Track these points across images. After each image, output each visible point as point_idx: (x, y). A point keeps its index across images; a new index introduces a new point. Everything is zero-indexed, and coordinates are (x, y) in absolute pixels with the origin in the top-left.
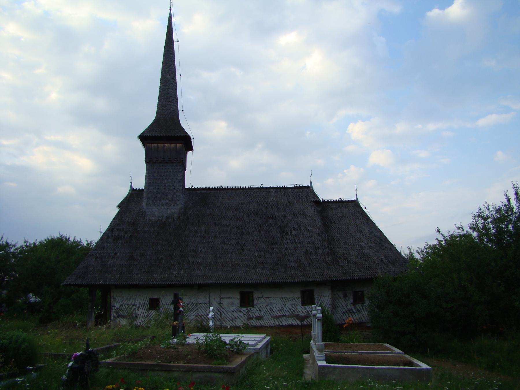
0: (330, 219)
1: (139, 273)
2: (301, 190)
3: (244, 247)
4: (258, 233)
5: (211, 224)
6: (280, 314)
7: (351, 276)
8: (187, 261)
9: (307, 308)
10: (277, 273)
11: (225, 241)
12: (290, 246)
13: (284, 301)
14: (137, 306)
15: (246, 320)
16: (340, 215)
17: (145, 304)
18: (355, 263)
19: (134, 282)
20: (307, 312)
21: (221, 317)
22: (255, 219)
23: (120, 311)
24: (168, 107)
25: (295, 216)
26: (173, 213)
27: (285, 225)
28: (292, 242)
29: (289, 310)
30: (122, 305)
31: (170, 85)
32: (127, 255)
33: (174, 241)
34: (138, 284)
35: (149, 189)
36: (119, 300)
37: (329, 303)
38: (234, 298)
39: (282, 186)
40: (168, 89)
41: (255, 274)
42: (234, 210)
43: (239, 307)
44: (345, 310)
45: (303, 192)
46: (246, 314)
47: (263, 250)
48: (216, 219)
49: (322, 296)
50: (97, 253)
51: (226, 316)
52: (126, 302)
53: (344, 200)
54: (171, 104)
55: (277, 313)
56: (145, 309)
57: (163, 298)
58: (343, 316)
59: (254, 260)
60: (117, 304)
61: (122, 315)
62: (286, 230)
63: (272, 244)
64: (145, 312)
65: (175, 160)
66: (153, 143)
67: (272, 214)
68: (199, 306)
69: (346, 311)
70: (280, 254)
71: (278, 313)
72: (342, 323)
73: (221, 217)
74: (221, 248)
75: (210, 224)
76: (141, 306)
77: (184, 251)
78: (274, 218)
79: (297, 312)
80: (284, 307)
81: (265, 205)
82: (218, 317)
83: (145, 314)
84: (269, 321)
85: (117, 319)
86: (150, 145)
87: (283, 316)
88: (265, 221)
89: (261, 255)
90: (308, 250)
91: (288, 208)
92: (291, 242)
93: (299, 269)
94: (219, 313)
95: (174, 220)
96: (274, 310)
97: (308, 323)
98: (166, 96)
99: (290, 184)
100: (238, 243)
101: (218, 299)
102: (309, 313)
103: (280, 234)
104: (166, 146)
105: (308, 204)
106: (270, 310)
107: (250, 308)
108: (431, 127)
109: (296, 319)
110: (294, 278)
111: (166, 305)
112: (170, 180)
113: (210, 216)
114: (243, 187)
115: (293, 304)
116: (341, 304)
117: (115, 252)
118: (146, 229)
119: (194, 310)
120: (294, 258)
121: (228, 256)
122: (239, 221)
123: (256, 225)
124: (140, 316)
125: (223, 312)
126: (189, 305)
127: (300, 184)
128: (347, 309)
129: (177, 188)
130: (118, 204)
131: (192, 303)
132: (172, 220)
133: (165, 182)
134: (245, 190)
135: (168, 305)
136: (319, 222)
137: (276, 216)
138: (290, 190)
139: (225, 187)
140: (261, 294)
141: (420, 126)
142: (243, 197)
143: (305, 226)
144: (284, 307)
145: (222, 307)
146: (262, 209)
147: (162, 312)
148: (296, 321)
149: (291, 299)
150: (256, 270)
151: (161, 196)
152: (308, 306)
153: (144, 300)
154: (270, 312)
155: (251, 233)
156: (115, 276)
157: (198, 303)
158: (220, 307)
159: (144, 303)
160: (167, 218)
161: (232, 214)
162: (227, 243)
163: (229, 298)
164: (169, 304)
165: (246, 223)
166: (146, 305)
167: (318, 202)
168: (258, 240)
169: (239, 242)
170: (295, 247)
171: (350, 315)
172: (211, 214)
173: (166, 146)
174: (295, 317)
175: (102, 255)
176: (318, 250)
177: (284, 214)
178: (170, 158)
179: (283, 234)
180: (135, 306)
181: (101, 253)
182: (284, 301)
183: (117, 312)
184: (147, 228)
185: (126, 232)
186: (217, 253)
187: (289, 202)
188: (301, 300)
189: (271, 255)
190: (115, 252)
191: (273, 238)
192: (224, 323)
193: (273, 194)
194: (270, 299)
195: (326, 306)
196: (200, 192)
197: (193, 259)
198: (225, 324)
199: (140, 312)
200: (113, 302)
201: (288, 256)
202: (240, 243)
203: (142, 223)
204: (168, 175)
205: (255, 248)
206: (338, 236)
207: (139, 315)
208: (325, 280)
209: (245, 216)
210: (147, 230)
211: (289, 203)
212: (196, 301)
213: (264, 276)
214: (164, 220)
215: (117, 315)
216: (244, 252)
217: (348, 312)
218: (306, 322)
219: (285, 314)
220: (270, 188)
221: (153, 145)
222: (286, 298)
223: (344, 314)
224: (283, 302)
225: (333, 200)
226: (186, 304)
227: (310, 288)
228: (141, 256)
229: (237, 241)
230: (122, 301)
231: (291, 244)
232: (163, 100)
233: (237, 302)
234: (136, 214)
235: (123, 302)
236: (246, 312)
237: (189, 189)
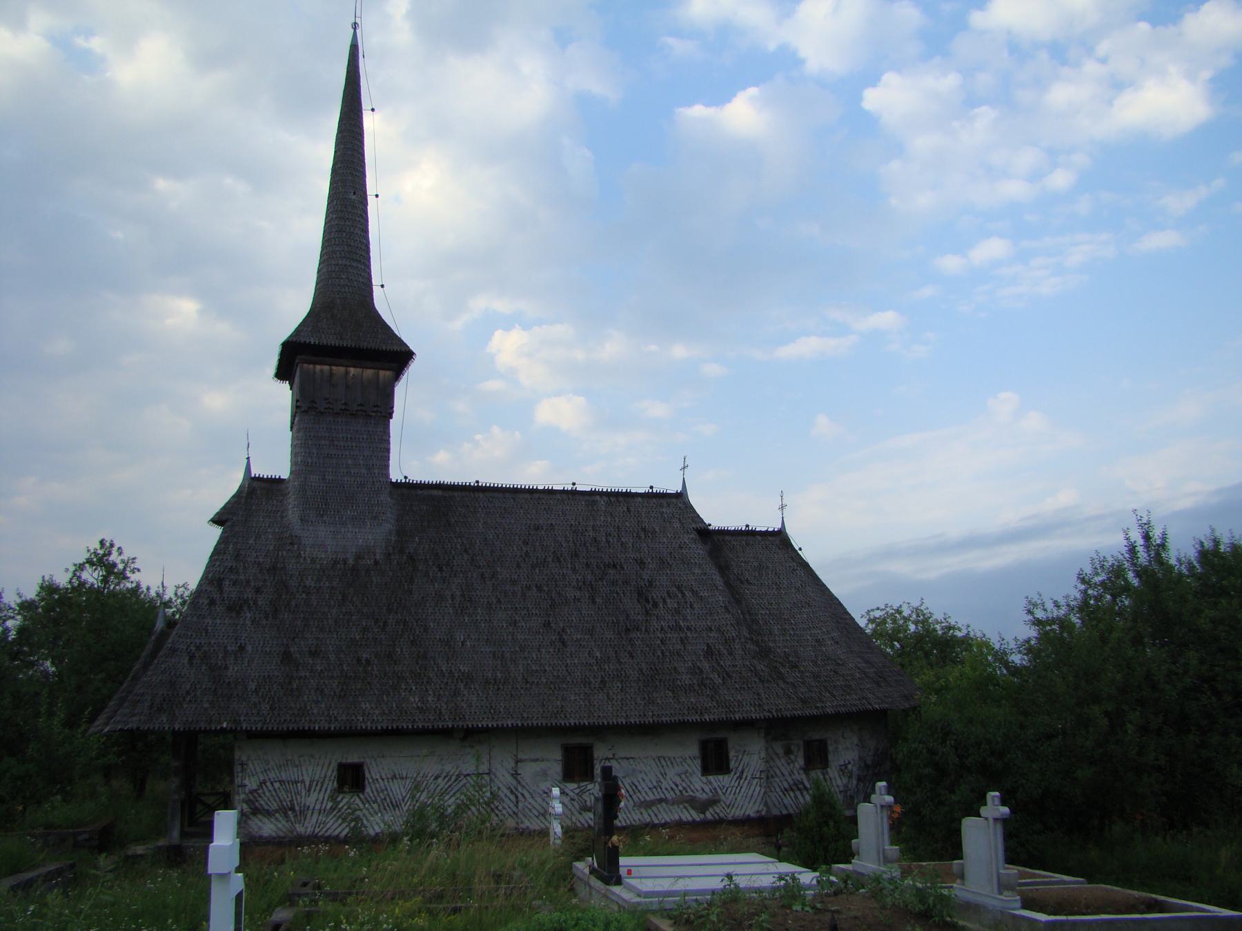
0: (735, 571)
1: (320, 699)
2: (664, 502)
5: (472, 577)
6: (654, 795)
7: (818, 707)
8: (436, 669)
9: (713, 780)
11: (516, 620)
12: (669, 635)
13: (663, 767)
14: (305, 785)
15: (576, 813)
16: (754, 563)
17: (325, 777)
18: (816, 677)
19: (314, 723)
20: (713, 791)
21: (517, 807)
22: (575, 568)
23: (259, 799)
24: (353, 273)
25: (664, 563)
26: (372, 544)
27: (647, 585)
28: (673, 625)
29: (674, 786)
30: (264, 782)
31: (357, 219)
32: (275, 651)
33: (391, 617)
34: (326, 728)
35: (308, 480)
36: (255, 769)
37: (760, 769)
38: (548, 760)
39: (620, 491)
41: (610, 703)
42: (520, 543)
43: (560, 783)
44: (789, 783)
46: (576, 797)
47: (611, 645)
49: (746, 753)
51: (530, 803)
52: (275, 773)
53: (757, 530)
56: (326, 791)
57: (374, 764)
58: (784, 797)
59: (596, 668)
61: (264, 809)
62: (652, 597)
63: (628, 630)
64: (326, 798)
66: (321, 364)
67: (612, 556)
68: (465, 781)
69: (790, 786)
72: (781, 812)
73: (494, 561)
74: (510, 637)
76: (317, 785)
77: (420, 642)
78: (618, 567)
79: (692, 791)
80: (662, 780)
82: (510, 807)
83: (327, 804)
85: (250, 819)
86: (311, 366)
87: (661, 801)
88: (599, 573)
89: (609, 657)
90: (710, 644)
92: (669, 626)
94: (513, 798)
95: (376, 563)
96: (640, 788)
98: (347, 245)
99: (639, 486)
100: (547, 625)
101: (510, 764)
102: (717, 792)
103: (639, 606)
104: (352, 373)
105: (685, 535)
106: (631, 786)
108: (679, 351)
110: (701, 713)
111: (380, 780)
112: (362, 460)
113: (466, 557)
114: (531, 487)
115: (682, 773)
116: (780, 770)
117: (241, 644)
119: (451, 791)
121: (533, 658)
122: (537, 571)
123: (582, 583)
124: (314, 809)
125: (522, 795)
126: (440, 780)
127: (660, 487)
128: (791, 782)
129: (380, 482)
130: (211, 516)
131: (448, 773)
132: (373, 563)
133: (349, 465)
134: (536, 496)
137: (623, 561)
138: (640, 499)
139: (488, 485)
140: (611, 749)
141: (653, 348)
142: (534, 511)
143: (691, 588)
145: (519, 783)
146: (585, 544)
148: (688, 811)
150: (608, 693)
151: (338, 499)
152: (715, 776)
153: (325, 768)
154: (632, 793)
155: (572, 601)
157: (462, 775)
158: (514, 783)
159: (322, 776)
160: (358, 557)
161: (519, 554)
162: (522, 626)
163: (536, 760)
166: (330, 780)
167: (705, 533)
168: (594, 620)
169: (549, 623)
170: (681, 638)
171: (798, 793)
172: (466, 551)
173: (352, 373)
174: (687, 803)
175: (207, 649)
176: (734, 645)
177: (639, 557)
178: (361, 405)
179: (648, 607)
180: (299, 784)
181: (200, 643)
182: (663, 767)
183: (251, 800)
185: (258, 591)
186: (504, 649)
187: (644, 530)
188: (699, 761)
189: (632, 657)
190: (241, 644)
191: (628, 614)
193: (603, 508)
194: (631, 761)
195: (754, 776)
196: (426, 492)
197: (448, 664)
198: (527, 823)
199: (314, 800)
200: (240, 775)
201: (671, 659)
202: (552, 625)
203: (295, 567)
204: (356, 447)
205: (590, 640)
206: (763, 612)
207: (311, 808)
208: (769, 716)
209: (550, 560)
210: (313, 585)
211: (645, 531)
212: (457, 768)
213: (632, 707)
214: (351, 562)
215: (251, 808)
216: (567, 649)
217: (794, 788)
218: (711, 813)
219: (664, 797)
220: (592, 493)
221: (318, 367)
222: (667, 759)
223: (785, 792)
224: (661, 768)
225: (733, 529)
226: (433, 778)
228: (314, 654)
229: (545, 621)
230: (265, 771)
231: (672, 629)
235: (268, 775)
236: (578, 794)
237: (397, 485)
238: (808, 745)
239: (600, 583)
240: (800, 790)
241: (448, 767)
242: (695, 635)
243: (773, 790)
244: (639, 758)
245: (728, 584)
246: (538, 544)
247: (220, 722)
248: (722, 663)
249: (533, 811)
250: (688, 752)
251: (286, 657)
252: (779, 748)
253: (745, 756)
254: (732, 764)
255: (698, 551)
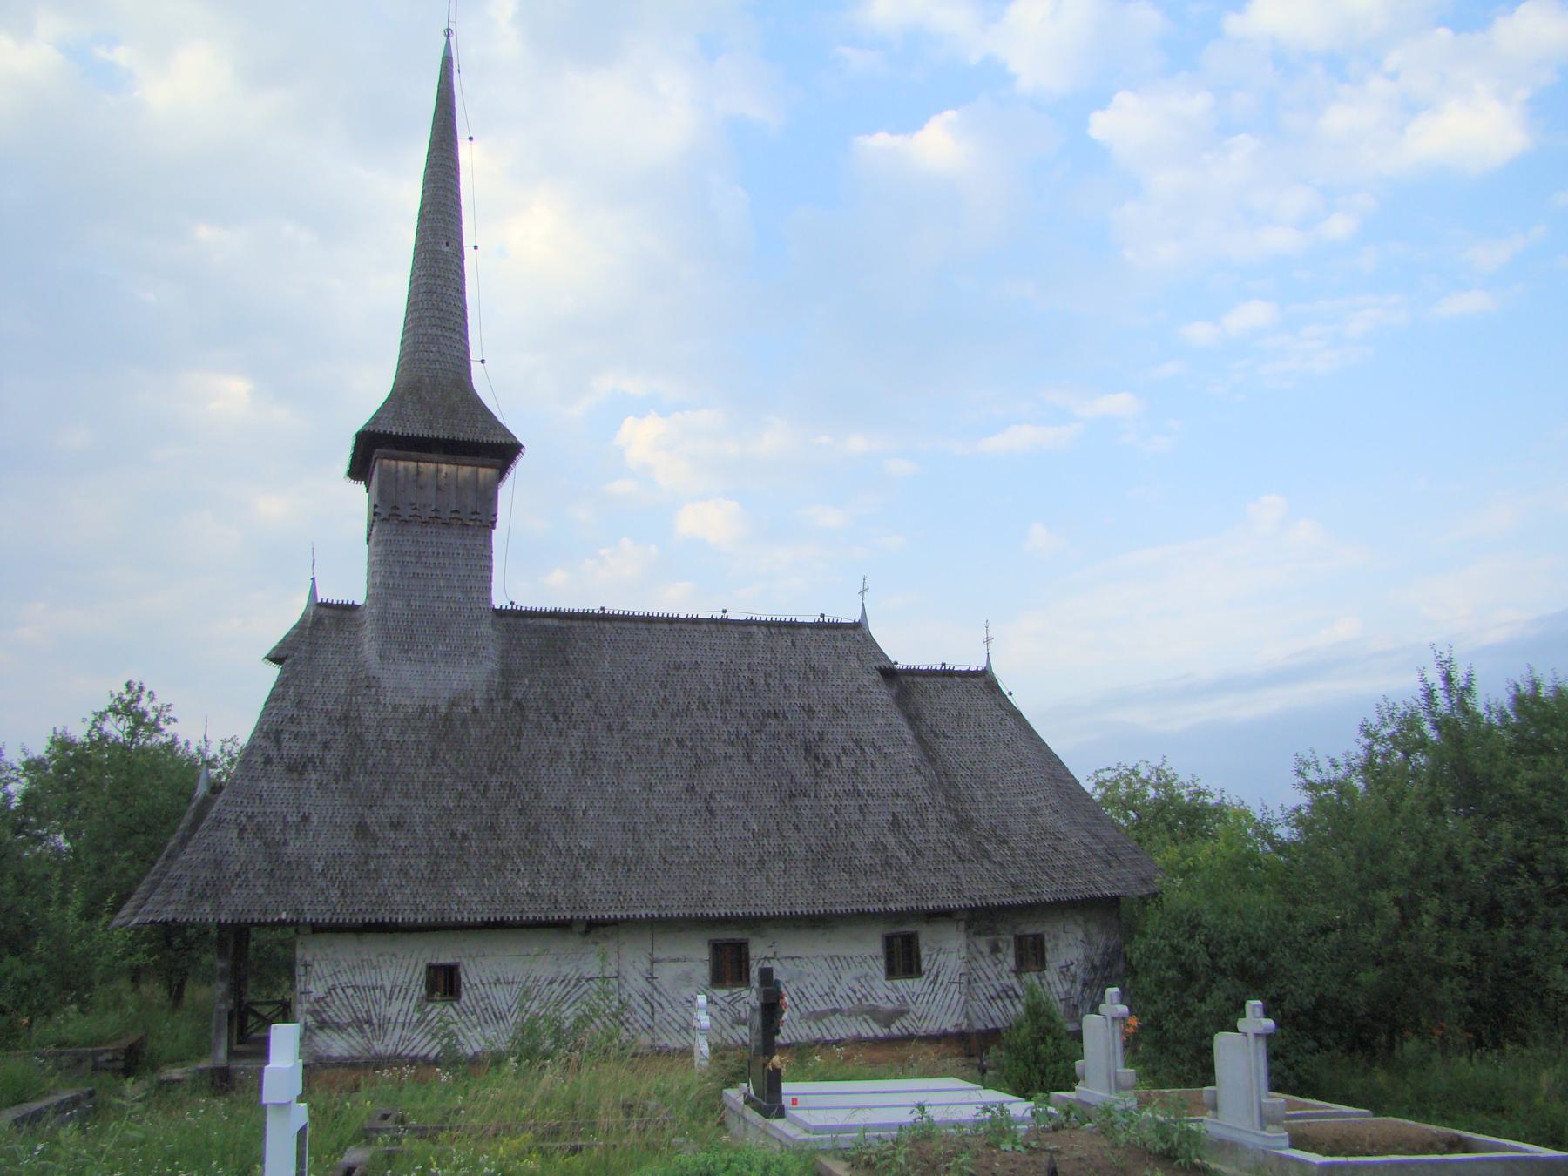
2: (838, 633)
3: (712, 804)
4: (745, 759)
5: (596, 729)
10: (832, 885)
13: (837, 968)
14: (385, 992)
17: (410, 981)
18: (1030, 854)
21: (653, 1020)
23: (327, 1009)
26: (470, 687)
36: (322, 971)
38: (692, 961)
40: (444, 288)
42: (657, 686)
44: (996, 989)
45: (844, 639)
46: (727, 1007)
48: (607, 712)
50: (242, 812)
54: (453, 335)
55: (816, 1003)
59: (752, 844)
60: (315, 984)
63: (792, 796)
64: (411, 1009)
65: (474, 517)
66: (405, 459)
68: (586, 986)
69: (998, 994)
70: (822, 827)
71: (821, 1002)
74: (644, 805)
75: (593, 727)
76: (400, 991)
79: (874, 999)
80: (836, 985)
81: (746, 675)
82: (643, 1020)
84: (794, 1030)
85: (315, 1034)
86: (393, 462)
87: (834, 1011)
91: (814, 688)
93: (889, 872)
94: (647, 1008)
95: (475, 711)
96: (808, 995)
97: (904, 1030)
99: (807, 614)
101: (644, 965)
102: (905, 1001)
103: (807, 765)
107: (739, 989)
109: (870, 1021)
110: (886, 901)
111: (480, 986)
113: (588, 703)
118: (391, 735)
120: (866, 840)
122: (678, 721)
124: (396, 1022)
125: (660, 1004)
126: (555, 985)
128: (999, 988)
130: (267, 652)
134: (677, 626)
135: (487, 987)
136: (907, 734)
137: (786, 709)
138: (808, 631)
142: (674, 646)
144: (836, 985)
145: (656, 989)
146: (738, 687)
147: (468, 1008)
149: (856, 961)
150: (768, 876)
152: (903, 981)
153: (410, 971)
154: (797, 1001)
156: (326, 892)
158: (649, 988)
159: (407, 980)
160: (453, 704)
161: (655, 700)
163: (676, 960)
164: (491, 981)
165: (704, 729)
167: (890, 674)
169: (693, 787)
171: (1007, 1002)
174: (867, 1014)
175: (261, 819)
178: (456, 511)
180: (378, 991)
182: (837, 968)
183: (316, 1011)
184: (395, 736)
185: (326, 746)
187: (813, 669)
189: (797, 829)
192: (664, 1037)
193: (762, 642)
194: (797, 961)
196: (537, 622)
200: (303, 978)
207: (393, 1020)
209: (694, 707)
210: (395, 739)
217: (1003, 995)
219: (838, 1007)
220: (748, 623)
221: (402, 464)
222: (842, 959)
225: (925, 668)
227: (908, 928)
230: (335, 974)
231: (848, 795)
232: (427, 322)
233: (703, 971)
234: (345, 686)
235: (338, 979)
236: (729, 1003)
237: (501, 613)
238: (1020, 941)
239: (758, 736)
240: (1010, 998)
241: (568, 970)
242: (877, 803)
243: (976, 997)
244: (807, 957)
245: (919, 738)
246: (679, 687)
247: (278, 912)
248: (911, 838)
249: (673, 1024)
250: (869, 949)
251: (362, 830)
252: (983, 944)
253: (941, 955)
254: (924, 966)
255: (882, 695)
